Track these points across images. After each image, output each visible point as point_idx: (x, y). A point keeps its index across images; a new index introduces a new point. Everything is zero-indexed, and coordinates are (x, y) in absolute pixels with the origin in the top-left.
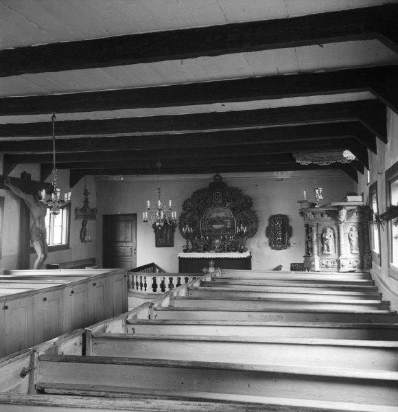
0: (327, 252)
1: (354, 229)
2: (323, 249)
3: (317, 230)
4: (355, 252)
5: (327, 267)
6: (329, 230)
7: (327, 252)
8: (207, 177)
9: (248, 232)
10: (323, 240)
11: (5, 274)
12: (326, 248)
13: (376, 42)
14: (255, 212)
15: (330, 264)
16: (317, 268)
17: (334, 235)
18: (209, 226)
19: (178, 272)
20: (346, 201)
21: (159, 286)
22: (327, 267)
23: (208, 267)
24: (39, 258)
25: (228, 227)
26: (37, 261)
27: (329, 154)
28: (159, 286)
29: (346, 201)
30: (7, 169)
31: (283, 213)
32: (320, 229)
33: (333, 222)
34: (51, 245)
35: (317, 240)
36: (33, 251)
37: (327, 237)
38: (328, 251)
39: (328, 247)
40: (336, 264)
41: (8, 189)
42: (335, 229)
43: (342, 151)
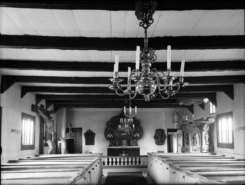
0: (196, 144)
1: (207, 133)
2: (193, 143)
3: (191, 134)
4: (207, 144)
5: (195, 150)
6: (197, 134)
7: (196, 144)
8: (119, 110)
9: (140, 136)
10: (194, 138)
11: (35, 156)
12: (195, 142)
13: (15, 83)
14: (142, 127)
15: (197, 149)
16: (191, 151)
17: (199, 136)
18: (120, 134)
19: (107, 155)
20: (208, 121)
21: (138, 162)
22: (195, 150)
23: (122, 153)
24: (50, 149)
25: (129, 134)
26: (49, 151)
27: (198, 100)
28: (138, 162)
29: (208, 121)
30: (37, 103)
31: (163, 128)
32: (192, 134)
33: (200, 131)
34: (25, 144)
35: (191, 139)
36: (47, 145)
37: (196, 137)
38: (196, 143)
39: (197, 142)
40: (200, 149)
41: (38, 112)
42: (200, 134)
43: (204, 99)
